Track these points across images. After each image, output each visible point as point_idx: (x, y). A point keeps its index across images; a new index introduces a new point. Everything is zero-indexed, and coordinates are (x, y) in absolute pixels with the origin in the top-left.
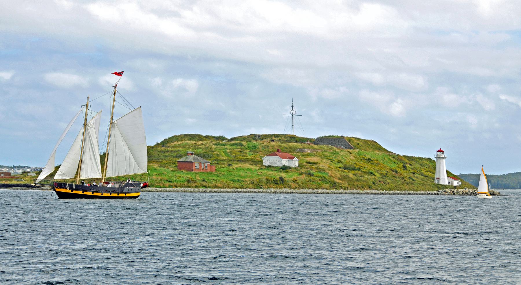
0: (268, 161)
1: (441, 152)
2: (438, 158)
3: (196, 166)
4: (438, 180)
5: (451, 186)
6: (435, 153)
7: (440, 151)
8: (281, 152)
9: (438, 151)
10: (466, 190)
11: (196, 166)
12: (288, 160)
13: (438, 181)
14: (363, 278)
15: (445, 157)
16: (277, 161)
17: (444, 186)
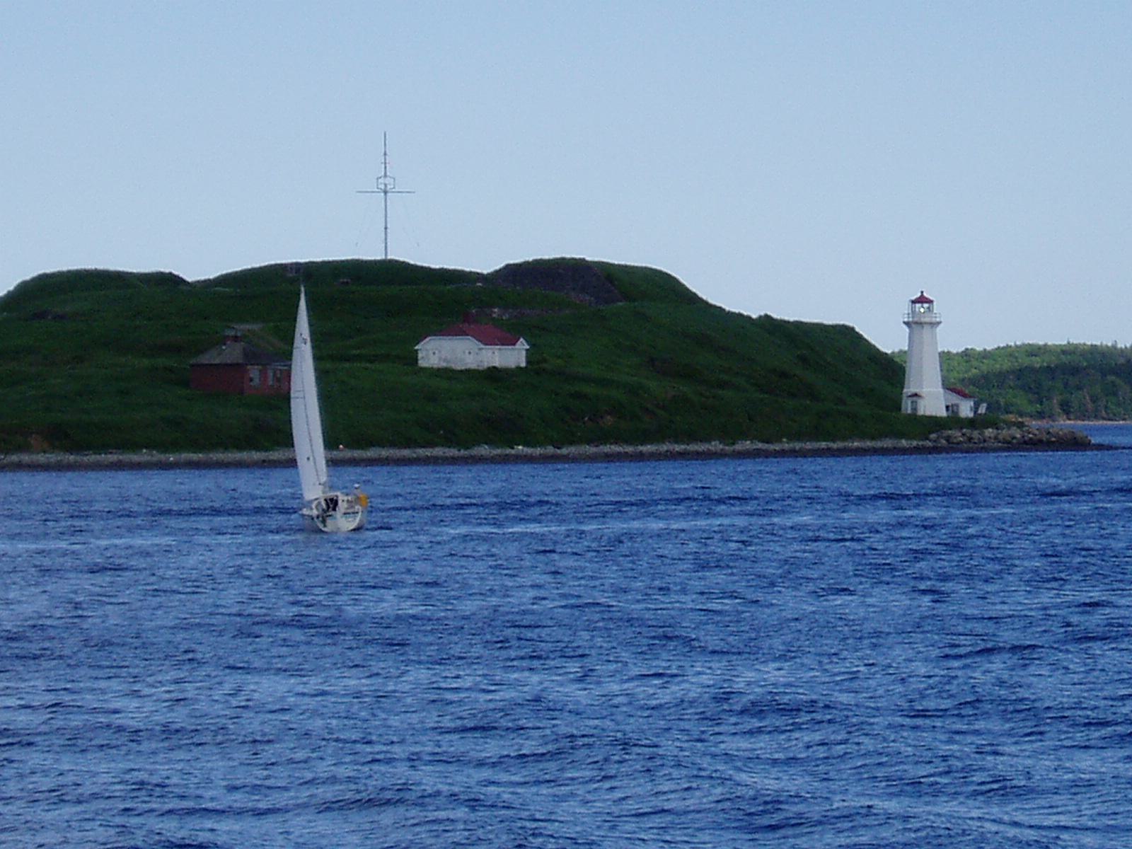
0: (434, 353)
1: (926, 302)
2: (916, 323)
3: (251, 380)
4: (916, 402)
5: (954, 420)
6: (906, 308)
7: (922, 300)
9: (914, 302)
11: (251, 380)
12: (500, 349)
16: (464, 352)
17: (934, 423)
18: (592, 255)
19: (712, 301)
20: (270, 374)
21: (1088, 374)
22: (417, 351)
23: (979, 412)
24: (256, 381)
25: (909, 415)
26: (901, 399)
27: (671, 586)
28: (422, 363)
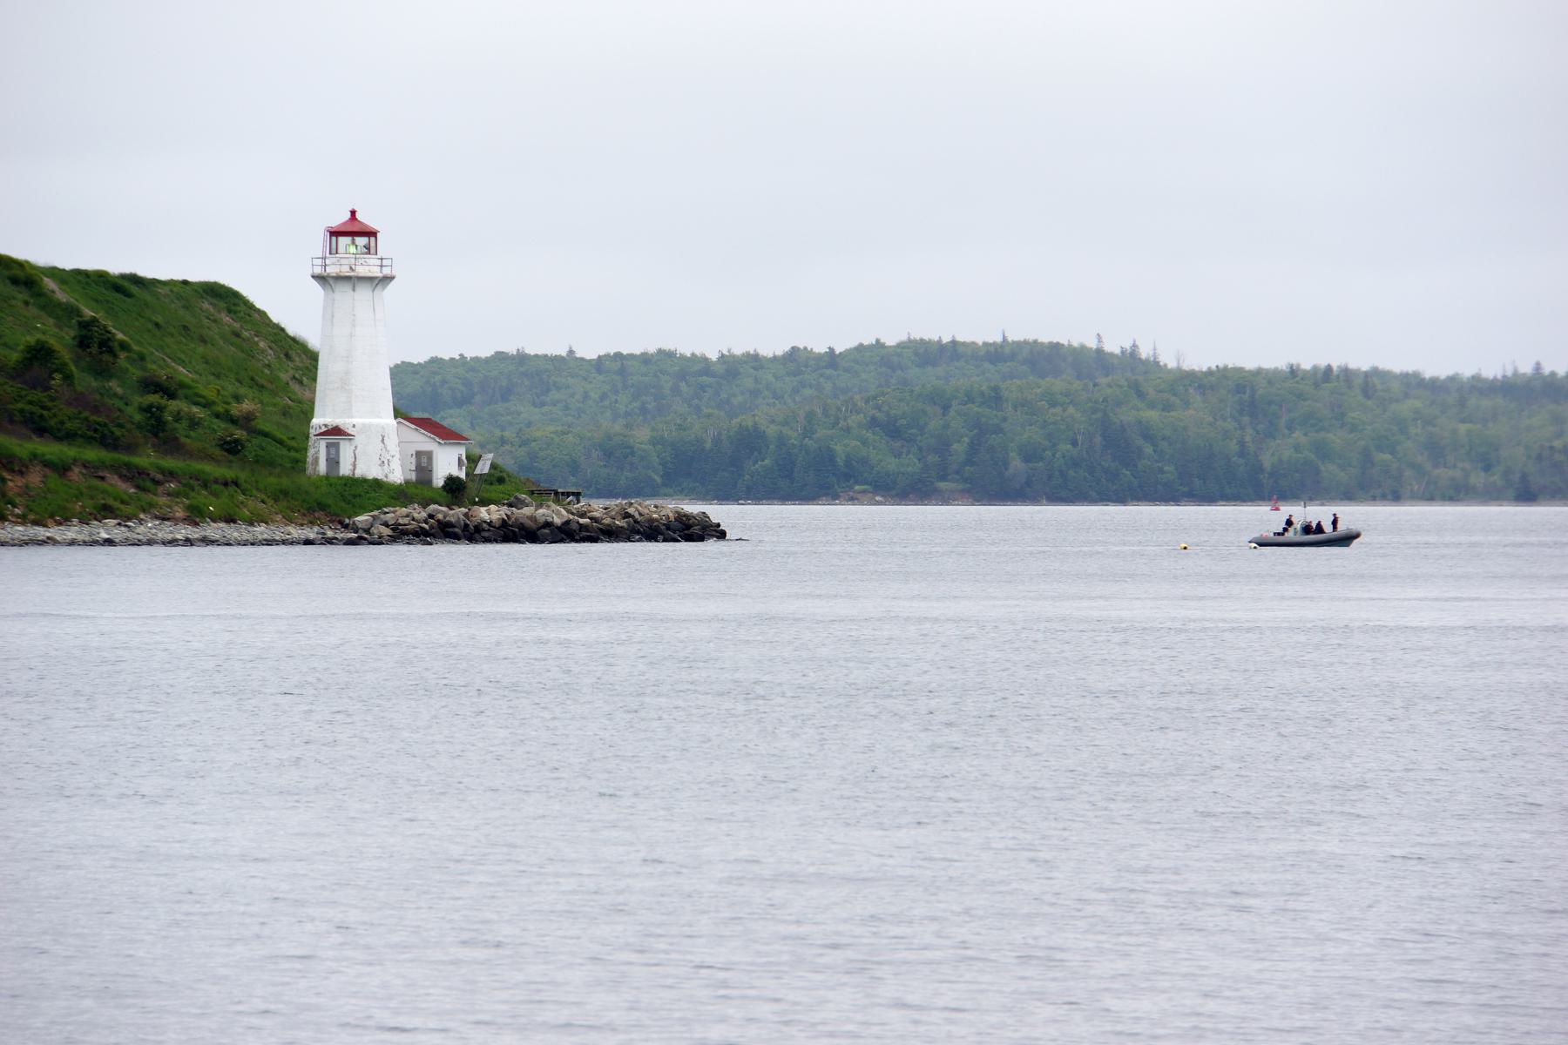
4: (337, 446)
6: (317, 242)
7: (354, 230)
9: (335, 233)
13: (333, 451)
14: (391, 640)
15: (387, 271)
19: (1436, 367)
23: (477, 471)
25: (321, 478)
26: (307, 437)
27: (740, 708)
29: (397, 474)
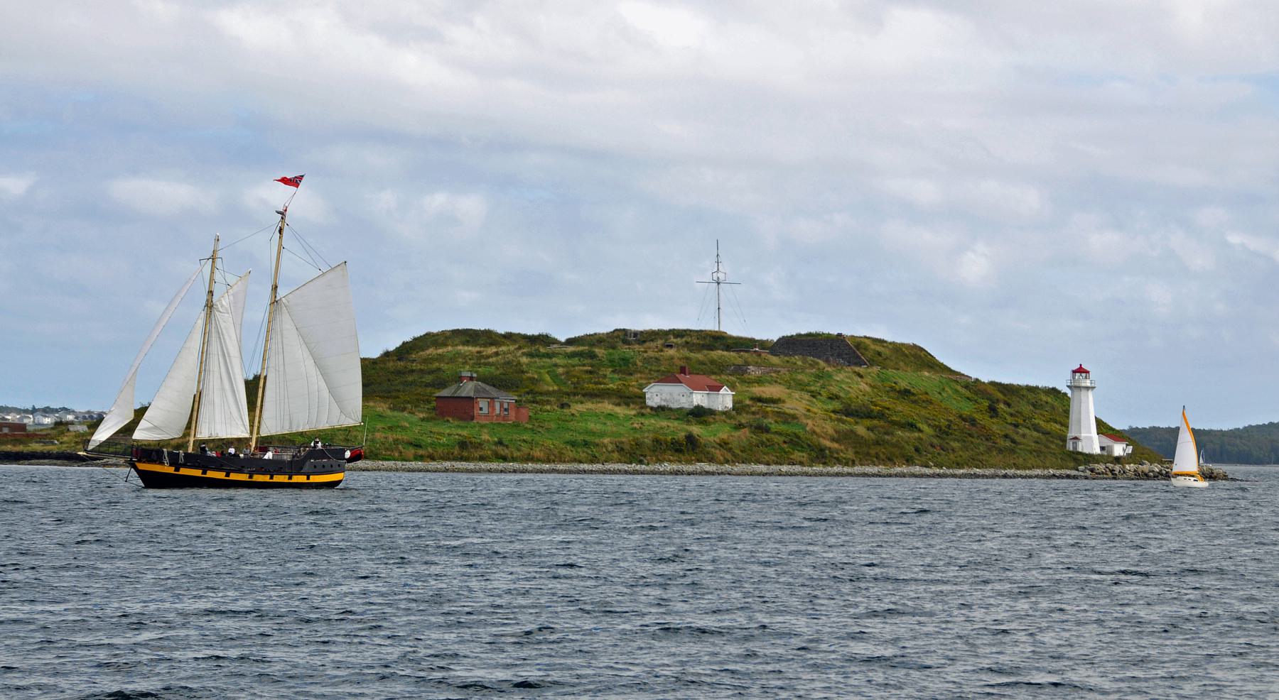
2: (1076, 387)
3: (481, 409)
5: (1106, 457)
6: (1069, 375)
7: (1080, 370)
8: (690, 374)
9: (1074, 372)
10: (1144, 466)
11: (481, 409)
15: (1093, 385)
17: (1090, 458)
18: (460, 328)
20: (497, 406)
21: (68, 430)
22: (645, 393)
24: (485, 411)
28: (649, 403)
29: (1097, 451)
